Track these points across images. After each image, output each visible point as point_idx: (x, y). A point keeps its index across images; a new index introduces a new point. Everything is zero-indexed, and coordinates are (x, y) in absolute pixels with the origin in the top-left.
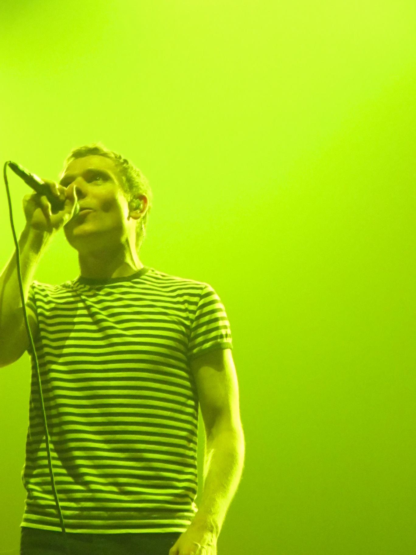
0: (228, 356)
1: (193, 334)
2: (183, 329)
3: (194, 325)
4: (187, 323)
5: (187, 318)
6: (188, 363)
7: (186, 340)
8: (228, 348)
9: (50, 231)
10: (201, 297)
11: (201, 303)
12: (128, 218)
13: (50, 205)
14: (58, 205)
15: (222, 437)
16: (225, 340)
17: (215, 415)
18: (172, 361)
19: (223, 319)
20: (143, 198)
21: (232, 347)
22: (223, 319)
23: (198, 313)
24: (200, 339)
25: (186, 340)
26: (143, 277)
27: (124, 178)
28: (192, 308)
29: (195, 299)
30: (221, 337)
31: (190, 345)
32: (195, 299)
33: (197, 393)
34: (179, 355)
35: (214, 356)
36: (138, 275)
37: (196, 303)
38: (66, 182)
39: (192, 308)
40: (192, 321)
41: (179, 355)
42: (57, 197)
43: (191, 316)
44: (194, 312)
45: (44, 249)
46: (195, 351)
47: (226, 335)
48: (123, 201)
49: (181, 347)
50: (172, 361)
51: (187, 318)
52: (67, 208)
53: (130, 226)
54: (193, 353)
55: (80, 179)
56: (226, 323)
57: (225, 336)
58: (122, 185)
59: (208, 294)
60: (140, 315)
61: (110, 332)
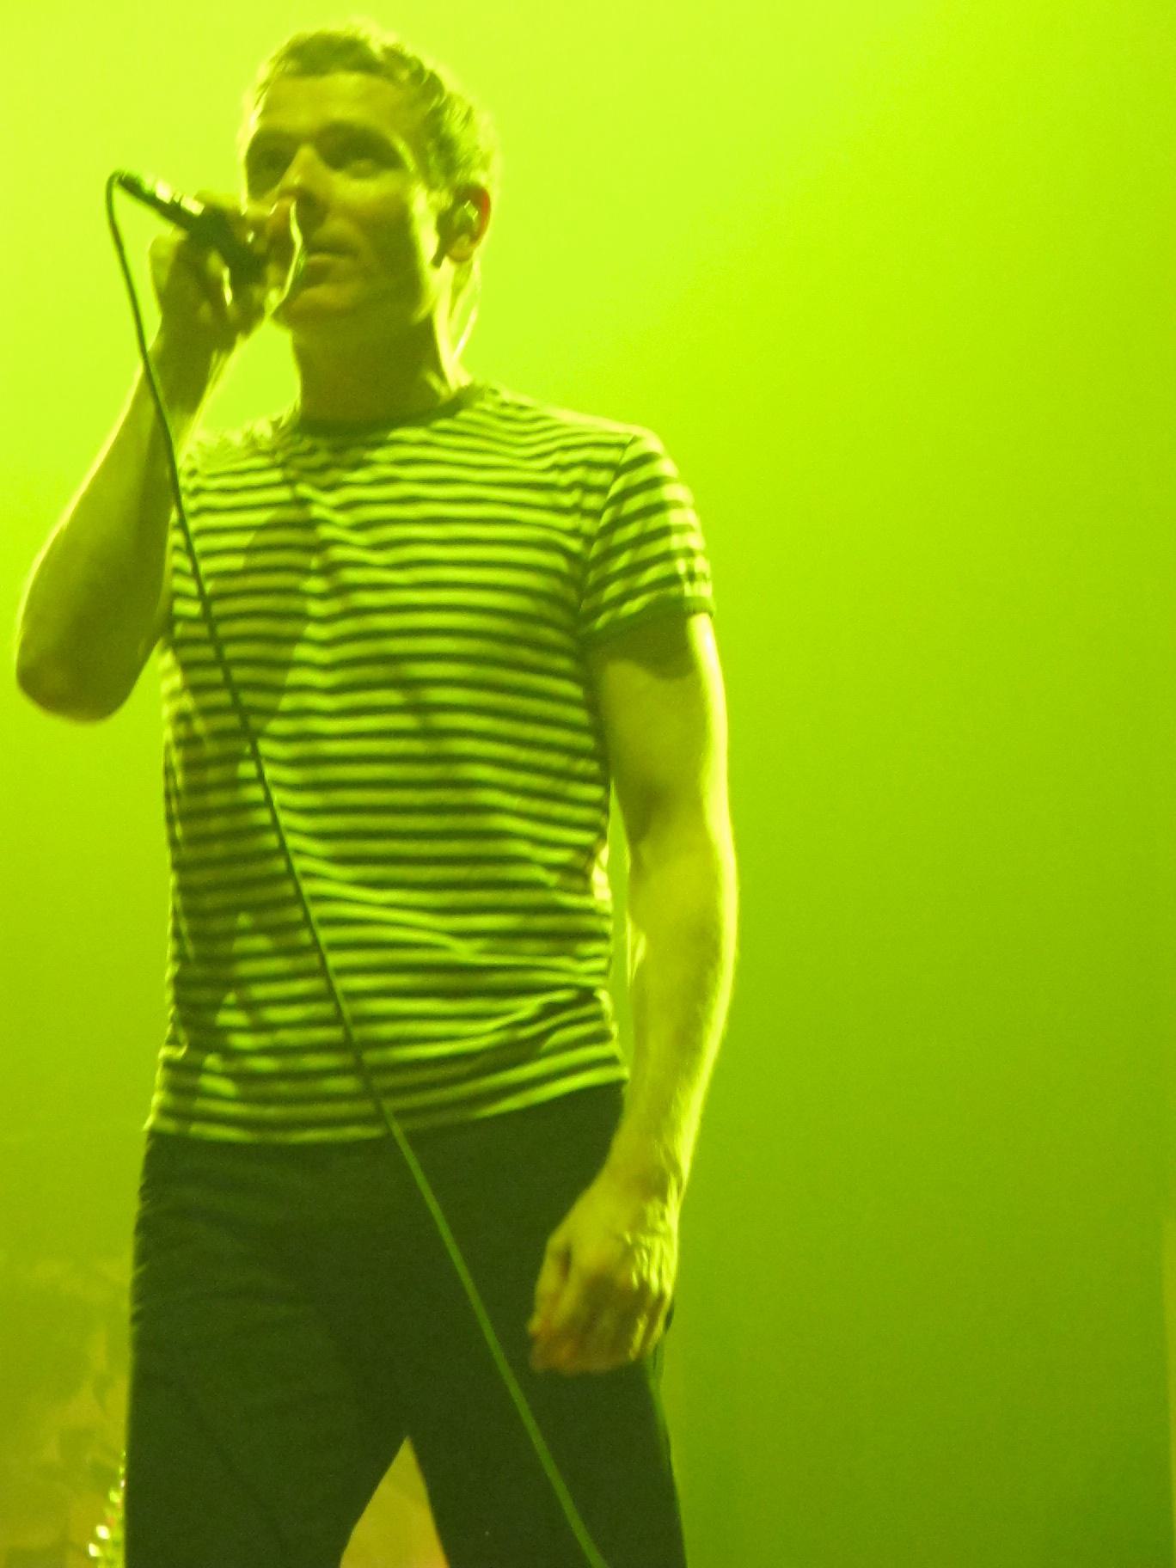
0: (702, 634)
1: (592, 577)
2: (559, 562)
3: (596, 549)
4: (575, 545)
5: (574, 533)
6: (579, 657)
7: (572, 595)
8: (694, 612)
9: (228, 345)
10: (618, 469)
11: (616, 488)
12: (437, 262)
13: (226, 274)
14: (249, 270)
15: (673, 879)
16: (688, 590)
17: (654, 807)
18: (525, 654)
19: (682, 529)
20: (479, 198)
21: (714, 609)
22: (682, 529)
23: (606, 518)
24: (614, 590)
25: (572, 595)
26: (463, 414)
27: (430, 145)
28: (593, 501)
29: (601, 478)
30: (674, 580)
31: (585, 606)
32: (601, 478)
33: (604, 755)
34: (550, 635)
35: (661, 638)
36: (455, 405)
37: (602, 490)
38: (268, 158)
39: (593, 501)
40: (589, 540)
41: (550, 635)
42: (246, 250)
43: (588, 525)
44: (596, 514)
45: (214, 395)
46: (601, 622)
47: (691, 577)
48: (424, 208)
49: (558, 614)
50: (525, 654)
51: (574, 533)
52: (272, 272)
53: (438, 280)
54: (596, 626)
55: (306, 153)
56: (695, 541)
57: (684, 579)
58: (425, 171)
59: (645, 459)
60: (442, 529)
61: (351, 576)
